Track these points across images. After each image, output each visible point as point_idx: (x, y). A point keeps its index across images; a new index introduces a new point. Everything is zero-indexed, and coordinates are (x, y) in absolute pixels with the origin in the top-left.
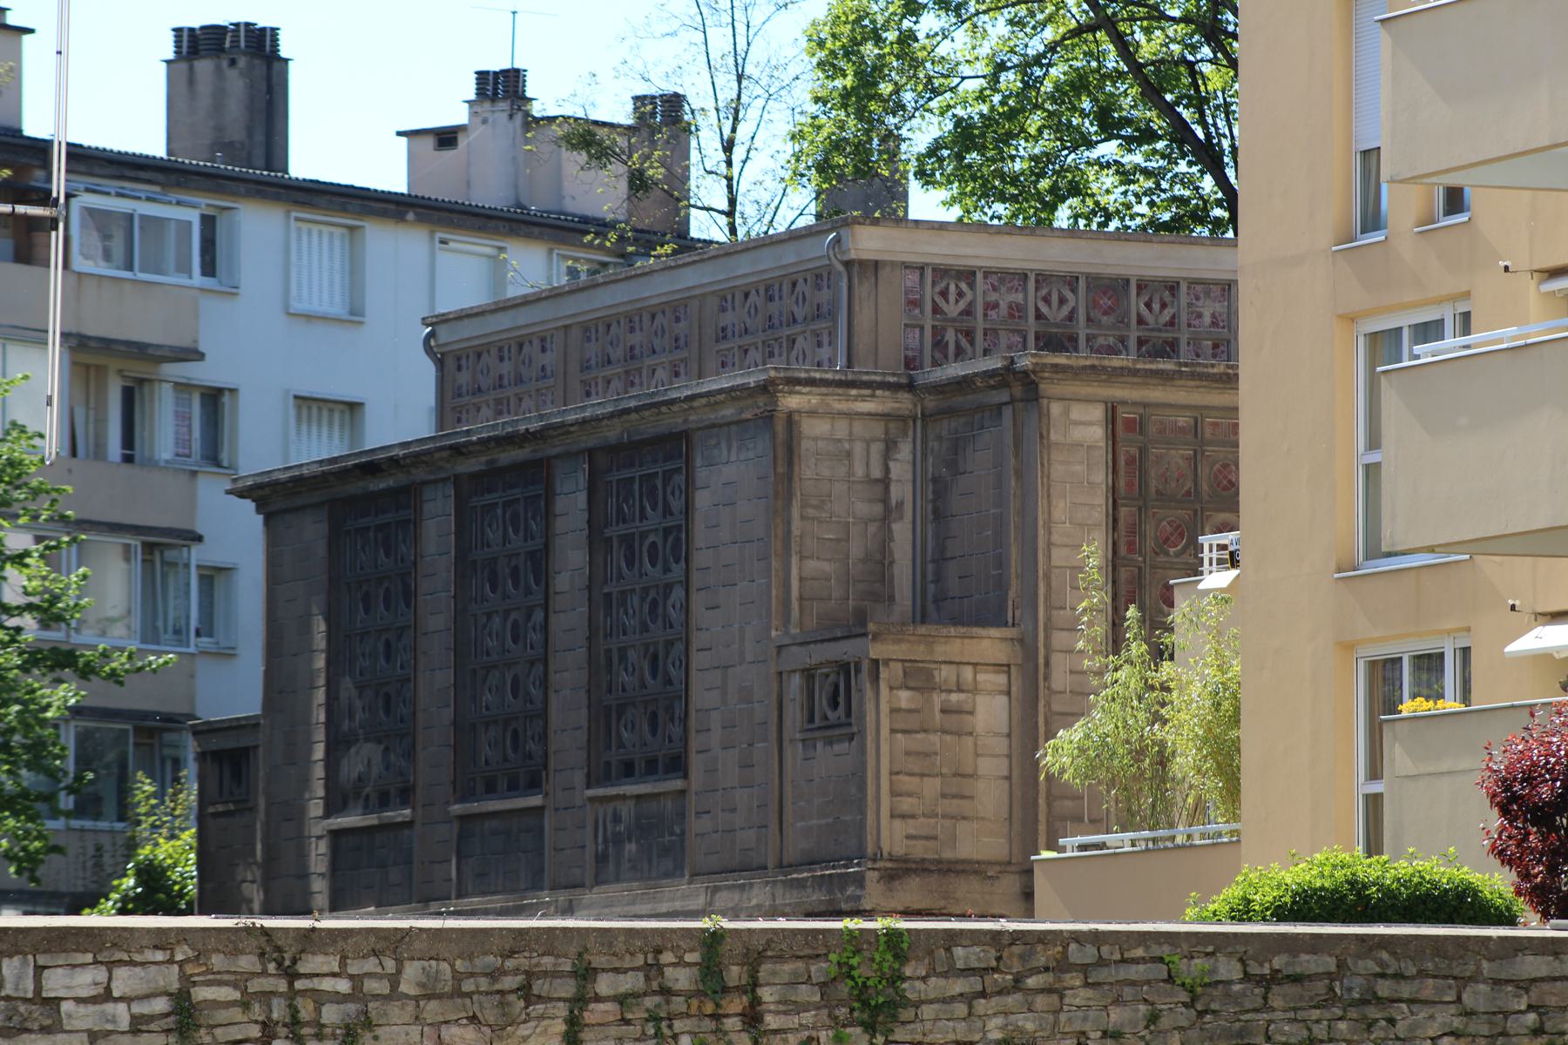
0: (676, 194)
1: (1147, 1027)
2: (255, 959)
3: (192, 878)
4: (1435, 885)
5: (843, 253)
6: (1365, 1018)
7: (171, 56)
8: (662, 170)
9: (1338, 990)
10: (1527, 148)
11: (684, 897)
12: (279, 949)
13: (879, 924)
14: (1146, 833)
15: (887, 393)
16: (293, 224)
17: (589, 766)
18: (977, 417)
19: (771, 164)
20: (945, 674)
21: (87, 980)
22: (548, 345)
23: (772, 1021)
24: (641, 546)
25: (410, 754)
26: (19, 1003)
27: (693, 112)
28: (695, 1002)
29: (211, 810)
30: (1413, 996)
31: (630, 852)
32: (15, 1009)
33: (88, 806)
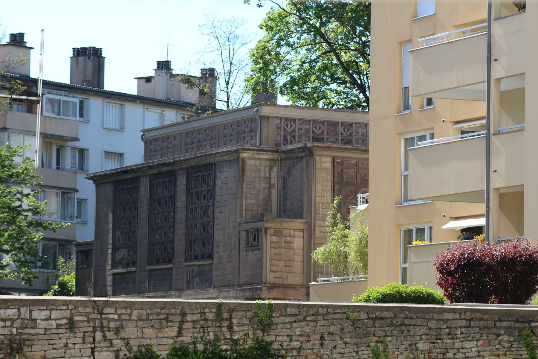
0: (212, 96)
1: (340, 332)
2: (91, 309)
5: (259, 114)
6: (401, 330)
7: (72, 56)
9: (394, 322)
11: (212, 293)
12: (98, 306)
13: (266, 302)
14: (341, 277)
15: (271, 153)
16: (105, 103)
18: (296, 160)
19: (239, 88)
20: (286, 232)
21: (44, 314)
22: (176, 138)
23: (236, 329)
24: (201, 195)
25: (135, 252)
27: (218, 73)
28: (214, 323)
32: (24, 322)
33: (45, 265)
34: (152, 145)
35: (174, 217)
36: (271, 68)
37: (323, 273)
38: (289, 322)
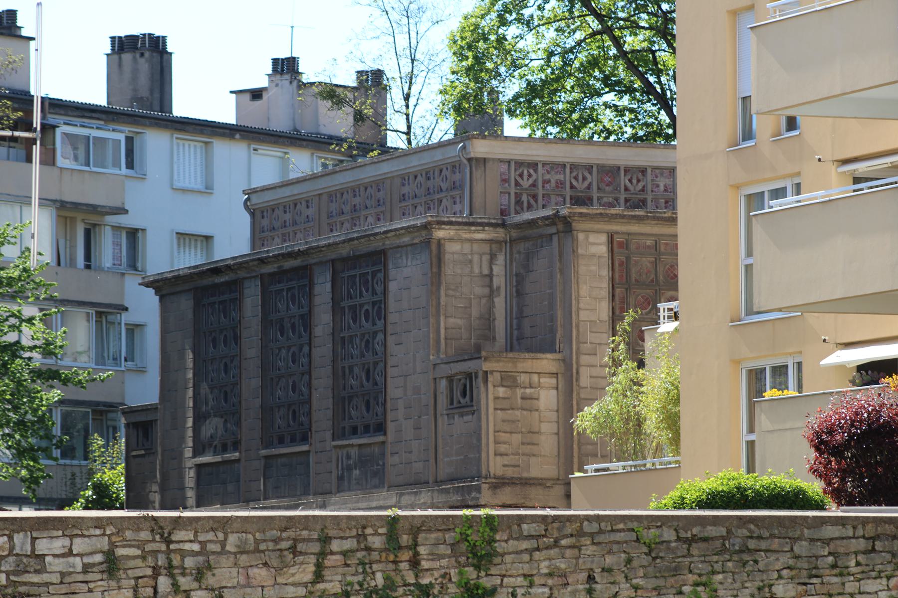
0: (379, 123)
1: (625, 566)
2: (148, 533)
3: (122, 490)
4: (782, 489)
5: (467, 154)
6: (741, 560)
7: (109, 52)
8: (371, 110)
9: (727, 546)
10: (829, 95)
11: (385, 499)
12: (161, 528)
13: (482, 512)
14: (630, 463)
15: (491, 229)
16: (175, 141)
17: (333, 429)
18: (539, 241)
19: (430, 107)
20: (523, 378)
21: (59, 545)
22: (310, 205)
23: (425, 564)
24: (360, 311)
25: (238, 423)
26: (23, 558)
27: (388, 79)
28: (384, 555)
29: (134, 453)
30: (768, 548)
31: (356, 474)
32: (21, 561)
33: (68, 452)
34: (265, 219)
35: (310, 355)
36: (490, 65)
37: (596, 456)
38: (526, 549)
